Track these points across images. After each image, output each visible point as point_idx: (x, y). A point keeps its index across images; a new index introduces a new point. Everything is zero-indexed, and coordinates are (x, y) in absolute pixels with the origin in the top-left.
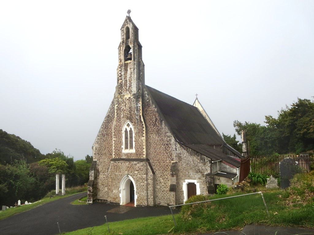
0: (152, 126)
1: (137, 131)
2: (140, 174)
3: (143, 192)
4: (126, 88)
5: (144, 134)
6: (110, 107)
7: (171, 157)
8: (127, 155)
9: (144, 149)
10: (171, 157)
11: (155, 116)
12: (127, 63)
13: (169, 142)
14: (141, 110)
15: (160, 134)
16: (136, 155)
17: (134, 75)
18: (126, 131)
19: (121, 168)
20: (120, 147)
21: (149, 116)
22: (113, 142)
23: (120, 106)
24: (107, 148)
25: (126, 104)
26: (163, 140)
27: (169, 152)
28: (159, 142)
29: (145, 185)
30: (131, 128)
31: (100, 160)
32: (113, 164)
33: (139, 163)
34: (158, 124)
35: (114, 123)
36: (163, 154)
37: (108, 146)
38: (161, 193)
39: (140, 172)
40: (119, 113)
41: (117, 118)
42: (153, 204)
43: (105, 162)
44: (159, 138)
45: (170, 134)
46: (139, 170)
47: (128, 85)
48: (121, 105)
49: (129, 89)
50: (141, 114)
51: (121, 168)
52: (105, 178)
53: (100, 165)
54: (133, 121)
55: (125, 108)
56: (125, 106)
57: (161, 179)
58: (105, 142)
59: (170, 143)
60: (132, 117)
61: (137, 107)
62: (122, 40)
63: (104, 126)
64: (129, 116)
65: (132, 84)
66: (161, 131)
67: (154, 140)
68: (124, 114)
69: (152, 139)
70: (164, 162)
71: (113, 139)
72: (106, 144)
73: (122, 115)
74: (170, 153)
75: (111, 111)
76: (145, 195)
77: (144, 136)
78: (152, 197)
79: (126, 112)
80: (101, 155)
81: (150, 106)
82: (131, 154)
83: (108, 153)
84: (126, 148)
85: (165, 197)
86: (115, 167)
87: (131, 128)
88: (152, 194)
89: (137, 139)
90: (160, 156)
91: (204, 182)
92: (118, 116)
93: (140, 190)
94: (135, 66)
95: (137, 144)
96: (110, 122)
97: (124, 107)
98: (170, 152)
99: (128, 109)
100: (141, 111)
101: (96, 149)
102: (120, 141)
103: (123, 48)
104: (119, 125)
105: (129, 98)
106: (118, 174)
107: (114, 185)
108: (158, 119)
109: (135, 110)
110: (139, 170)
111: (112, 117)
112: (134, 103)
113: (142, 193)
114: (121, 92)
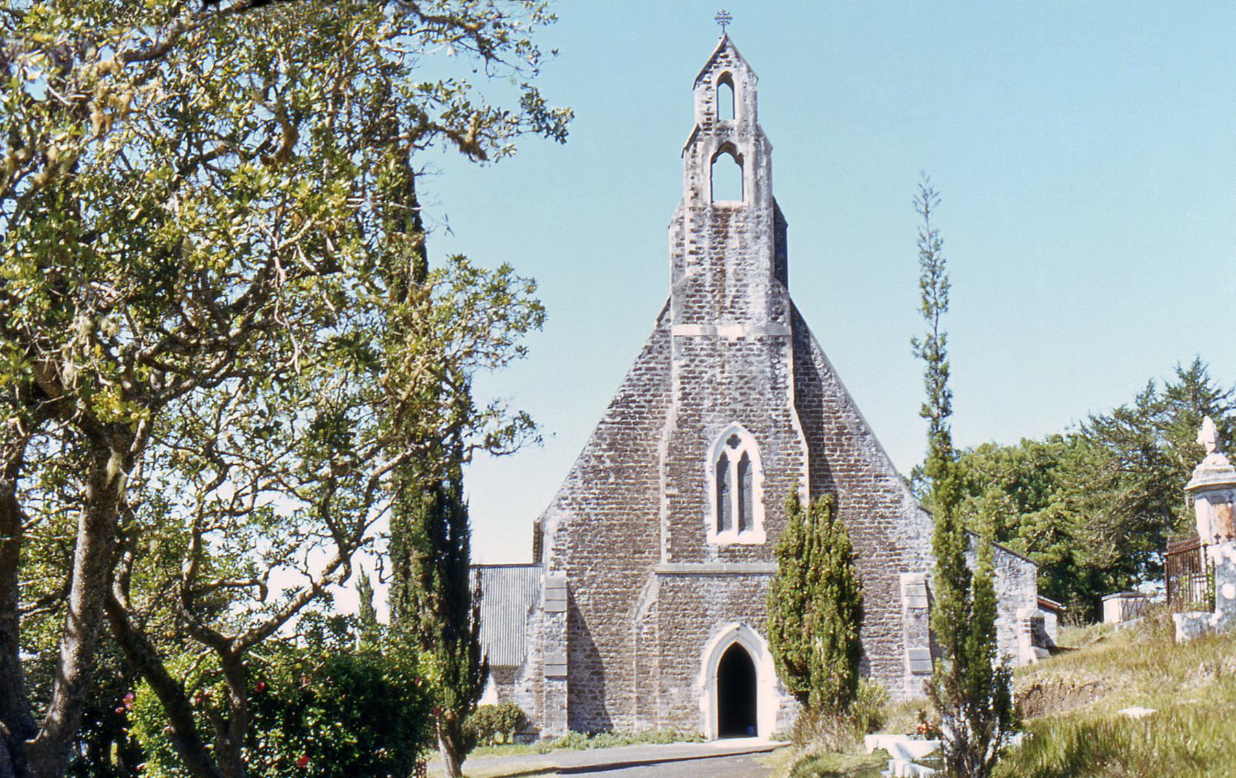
18: (723, 464)
21: (811, 412)
30: (745, 456)
40: (694, 392)
56: (723, 366)
59: (895, 513)
62: (704, 118)
65: (750, 290)
87: (745, 456)
97: (718, 370)
111: (643, 407)
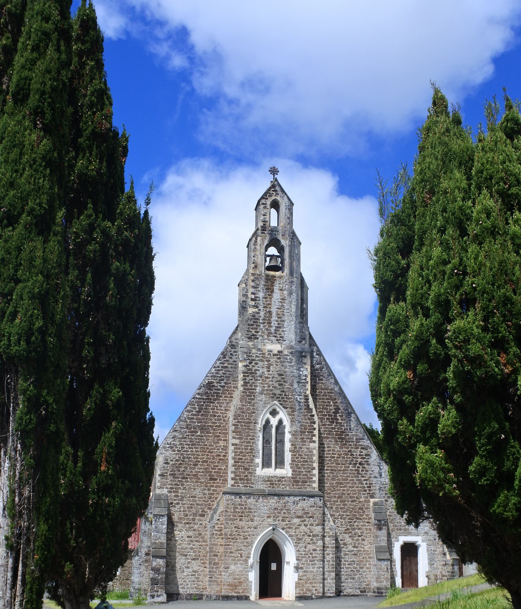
0: (328, 423)
1: (299, 429)
2: (306, 525)
3: (312, 565)
4: (267, 330)
5: (314, 435)
6: (215, 363)
7: (370, 490)
8: (268, 481)
9: (314, 468)
10: (370, 490)
11: (333, 403)
12: (274, 276)
13: (365, 460)
14: (309, 383)
15: (346, 441)
16: (294, 481)
17: (291, 307)
19: (254, 512)
20: (252, 463)
22: (231, 448)
23: (253, 366)
24: (201, 463)
25: (271, 365)
26: (352, 455)
27: (364, 480)
28: (343, 458)
29: (318, 549)
31: (178, 492)
32: (232, 500)
33: (304, 500)
34: (342, 420)
35: (236, 402)
36: (352, 484)
37: (205, 457)
38: (346, 568)
39: (308, 519)
40: (251, 382)
41: (243, 392)
42: (334, 591)
43: (195, 497)
44: (344, 449)
45: (368, 442)
46: (304, 516)
47: (274, 324)
48: (256, 364)
49: (276, 333)
50: (308, 392)
51: (254, 512)
52: (192, 539)
53: (178, 504)
54: (287, 405)
55: (266, 373)
56: (269, 368)
57: (347, 536)
58: (196, 448)
59: (367, 461)
60: (285, 395)
61: (300, 376)
63: (195, 408)
64: (278, 392)
65: (286, 324)
66: (348, 435)
67: (331, 452)
68: (264, 387)
69: (199, 450)
70: (352, 501)
71: (232, 441)
72: (200, 453)
73: (258, 388)
74: (368, 482)
75: (217, 373)
76: (317, 571)
77: (314, 442)
78: (333, 575)
79: (271, 383)
80: (183, 478)
81: (322, 380)
82: (281, 479)
83: (205, 475)
84: (266, 464)
85: (355, 575)
86: (237, 508)
87: (280, 422)
88: (333, 568)
89: (298, 447)
90: (345, 487)
91: (435, 539)
92: (248, 389)
93: (306, 561)
94: (294, 287)
95: (298, 458)
96: (215, 400)
97: (265, 370)
98: (367, 480)
99: (276, 376)
100: (309, 386)
101: (167, 463)
102: (251, 446)
103: (263, 240)
104: (248, 409)
105: (279, 352)
106: (246, 527)
107: (231, 553)
108: (341, 408)
109: (293, 382)
110: (304, 516)
111: (219, 390)
112: (292, 366)
113: (311, 567)
114: (253, 335)
